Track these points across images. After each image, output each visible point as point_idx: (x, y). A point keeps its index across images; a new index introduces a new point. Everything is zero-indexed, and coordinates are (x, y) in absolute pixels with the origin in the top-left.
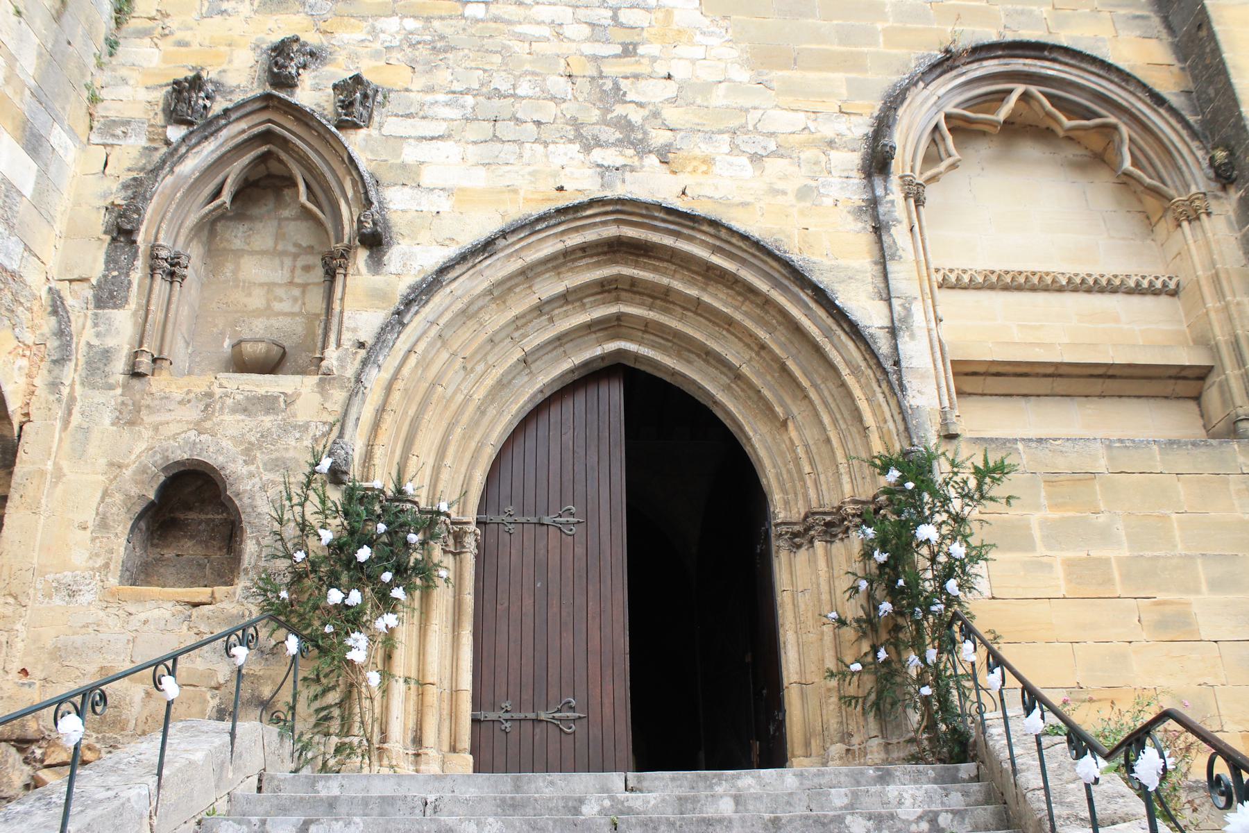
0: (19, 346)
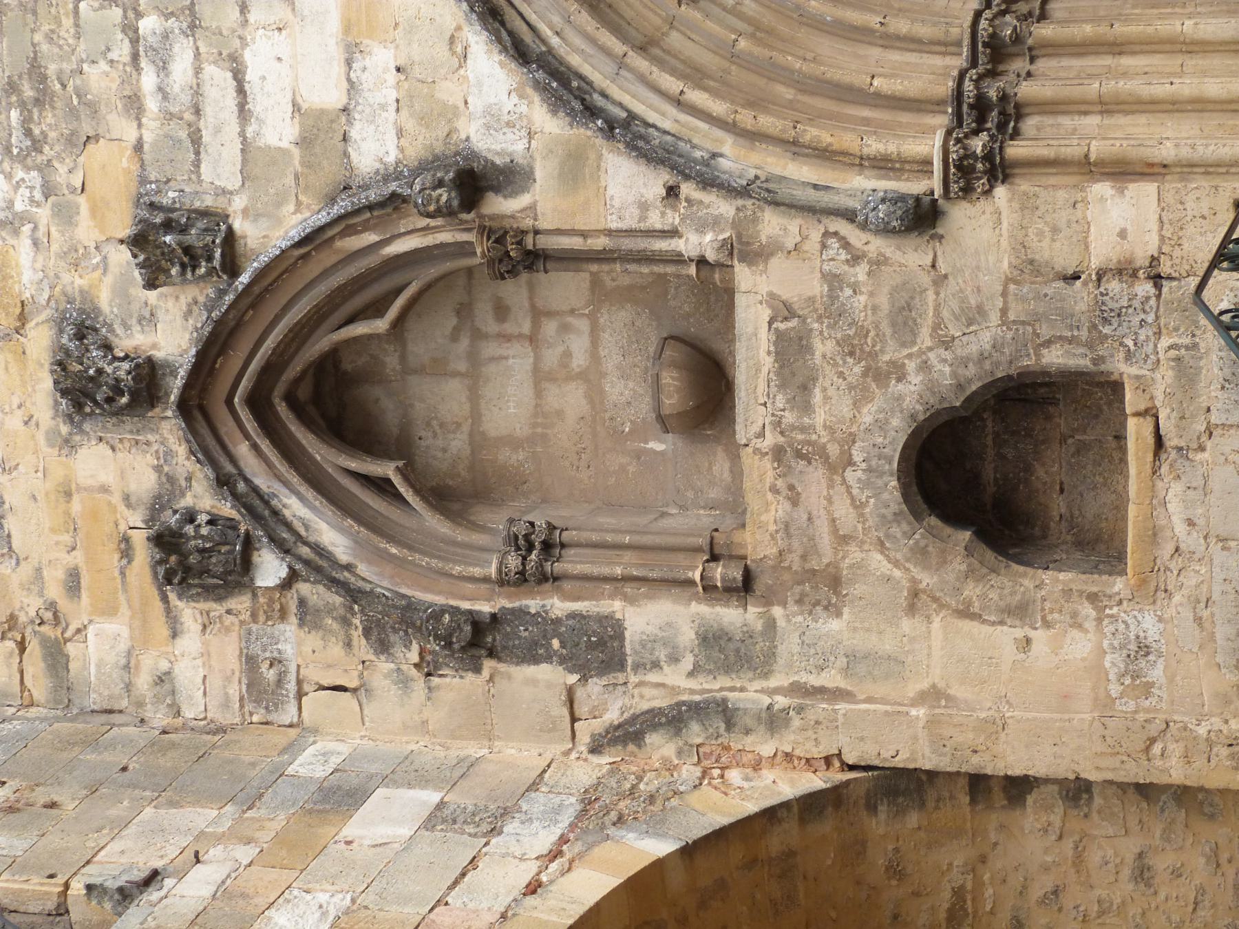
0: (709, 784)
